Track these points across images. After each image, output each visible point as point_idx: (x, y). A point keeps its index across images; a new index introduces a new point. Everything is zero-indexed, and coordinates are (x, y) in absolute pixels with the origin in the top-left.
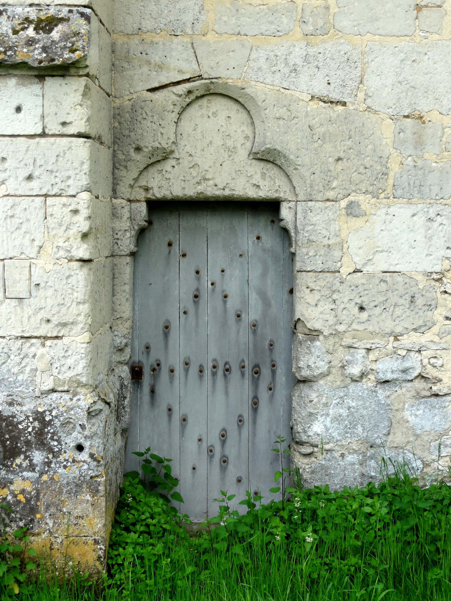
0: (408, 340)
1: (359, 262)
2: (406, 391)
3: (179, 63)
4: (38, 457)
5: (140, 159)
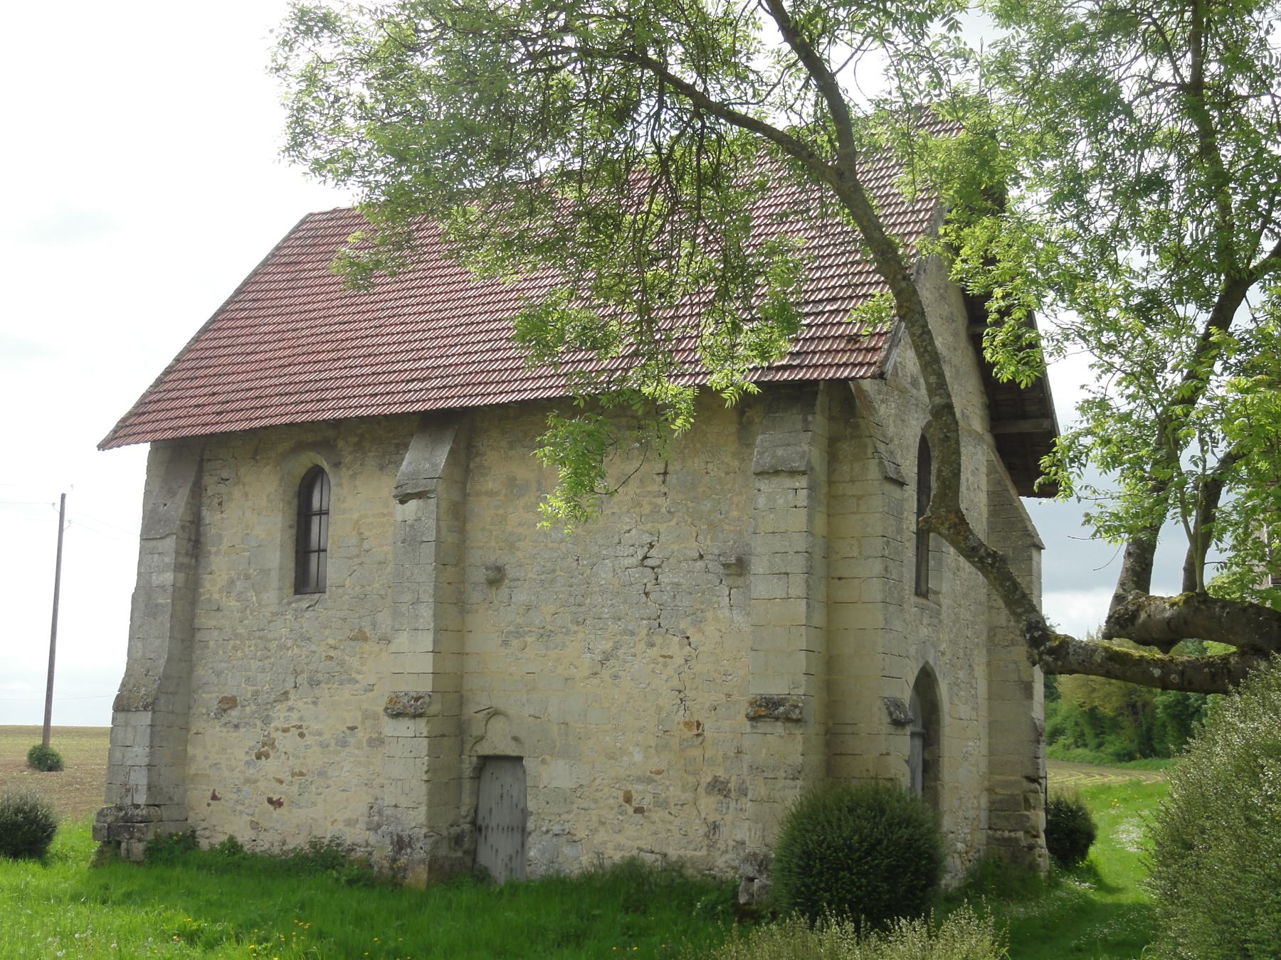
0: (564, 817)
1: (546, 783)
2: (563, 839)
3: (484, 702)
4: (409, 850)
5: (472, 740)
